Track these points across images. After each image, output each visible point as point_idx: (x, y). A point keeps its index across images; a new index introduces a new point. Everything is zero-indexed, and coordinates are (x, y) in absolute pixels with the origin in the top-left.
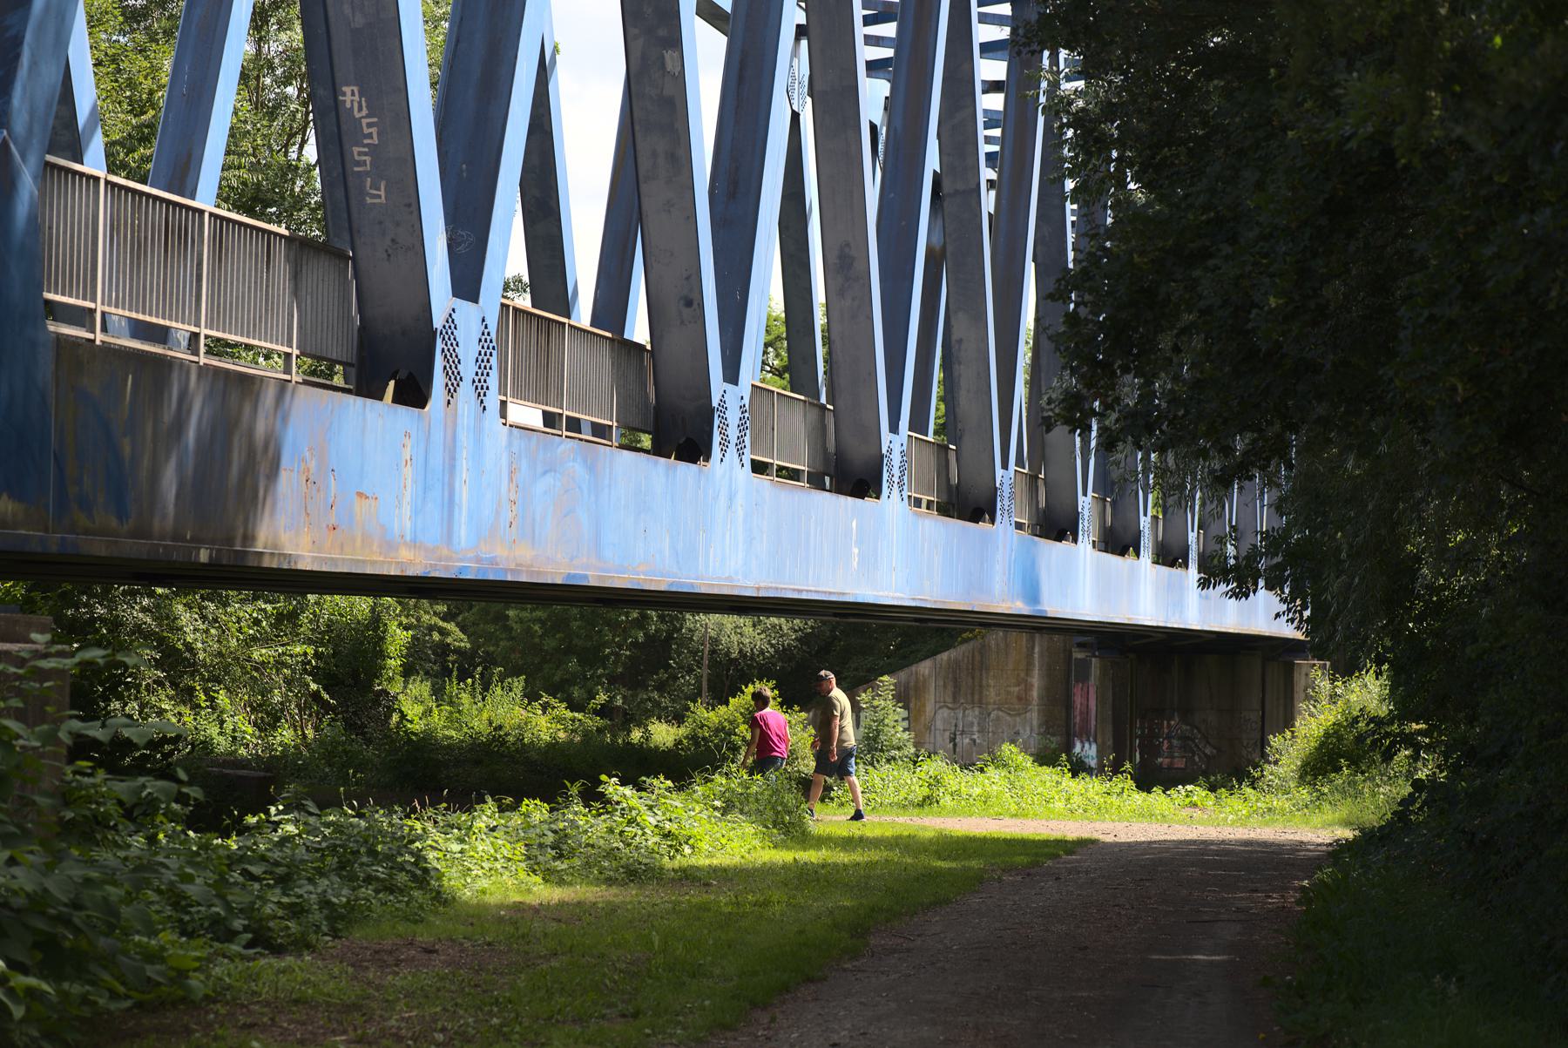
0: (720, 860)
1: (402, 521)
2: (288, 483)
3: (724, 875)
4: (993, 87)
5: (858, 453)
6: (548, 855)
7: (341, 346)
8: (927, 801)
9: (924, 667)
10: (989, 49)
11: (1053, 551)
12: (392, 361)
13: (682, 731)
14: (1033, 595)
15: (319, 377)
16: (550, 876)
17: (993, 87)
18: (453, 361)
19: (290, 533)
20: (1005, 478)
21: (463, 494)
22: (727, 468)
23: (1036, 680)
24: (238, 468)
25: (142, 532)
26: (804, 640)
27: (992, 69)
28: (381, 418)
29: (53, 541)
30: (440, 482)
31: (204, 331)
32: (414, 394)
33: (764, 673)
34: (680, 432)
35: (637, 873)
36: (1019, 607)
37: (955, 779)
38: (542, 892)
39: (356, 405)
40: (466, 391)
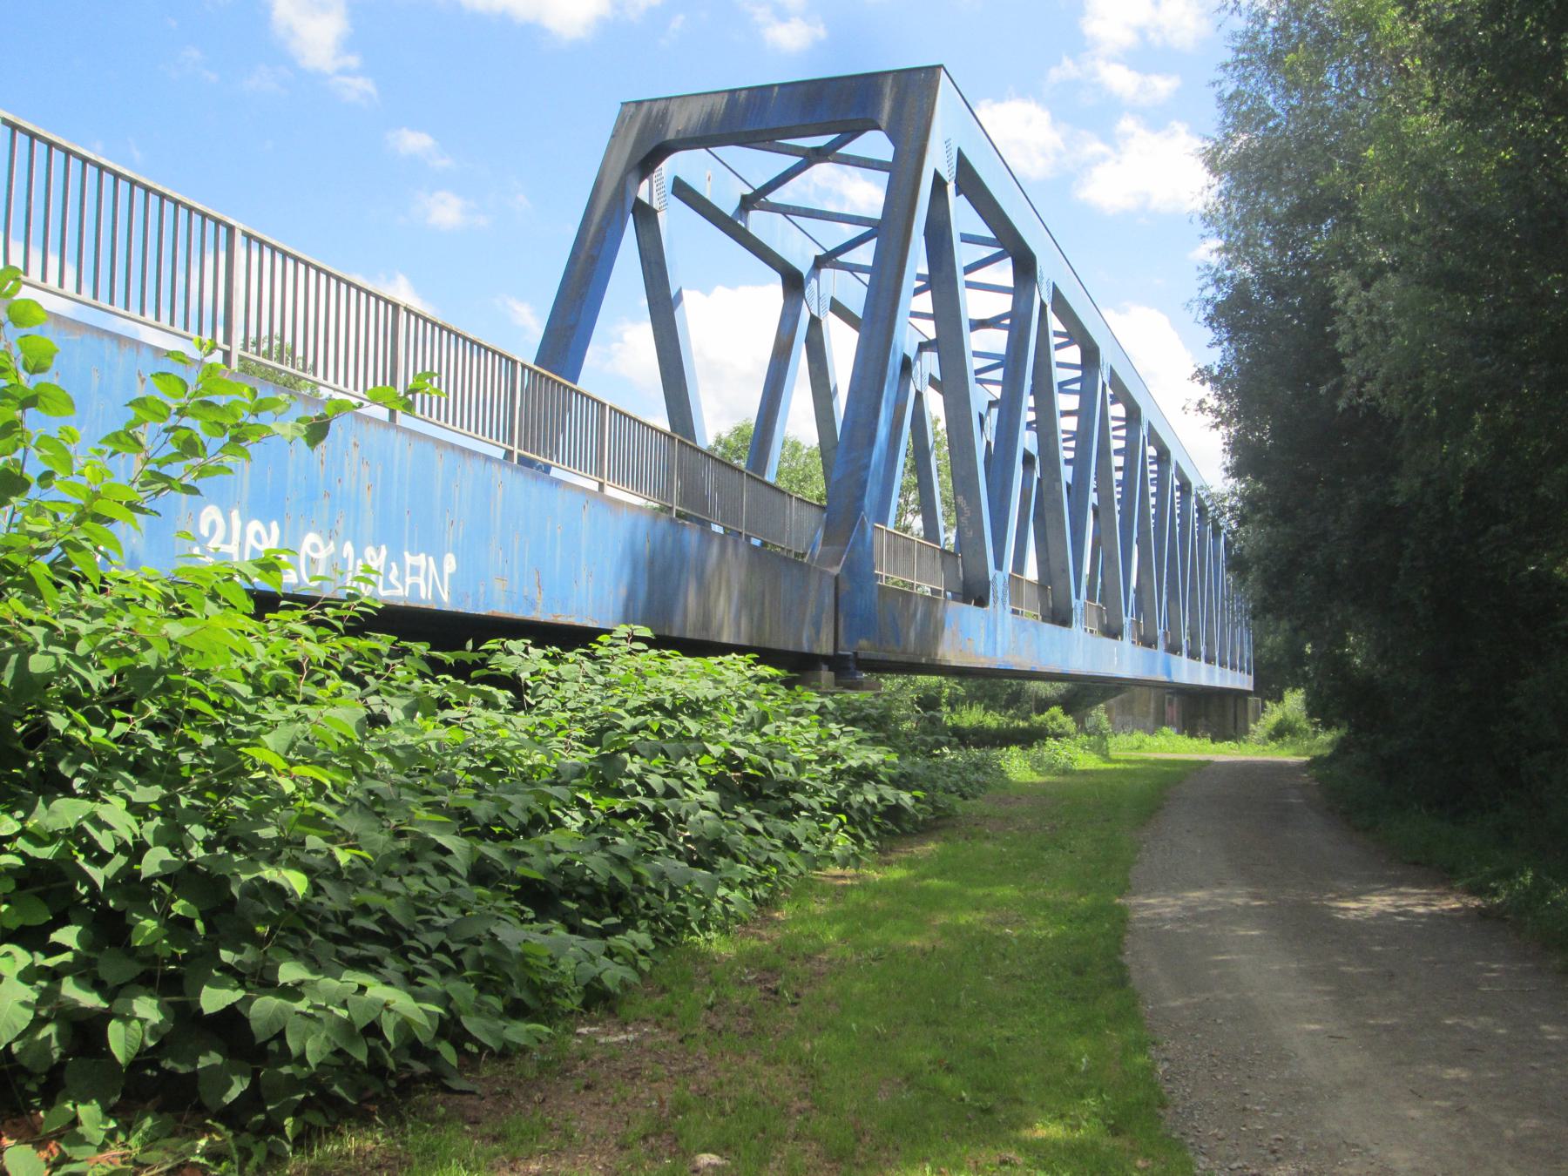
0: (1087, 767)
1: (981, 649)
2: (947, 634)
3: (1085, 773)
4: (1117, 452)
5: (1114, 625)
6: (1037, 764)
7: (958, 589)
8: (1139, 747)
9: (1112, 701)
10: (1117, 452)
11: (1174, 658)
12: (975, 593)
13: (238, 957)
14: (1169, 674)
15: (954, 598)
16: (1039, 773)
17: (1118, 469)
18: (995, 592)
19: (949, 653)
20: (1160, 632)
21: (999, 639)
22: (1077, 629)
23: (1152, 705)
24: (932, 630)
25: (904, 652)
26: (1068, 691)
27: (1118, 461)
28: (971, 610)
29: (880, 655)
30: (992, 633)
31: (516, 451)
32: (982, 602)
33: (1054, 703)
34: (1060, 616)
35: (1066, 772)
36: (1164, 678)
37: (1148, 739)
38: (1038, 779)
39: (965, 606)
40: (999, 603)
